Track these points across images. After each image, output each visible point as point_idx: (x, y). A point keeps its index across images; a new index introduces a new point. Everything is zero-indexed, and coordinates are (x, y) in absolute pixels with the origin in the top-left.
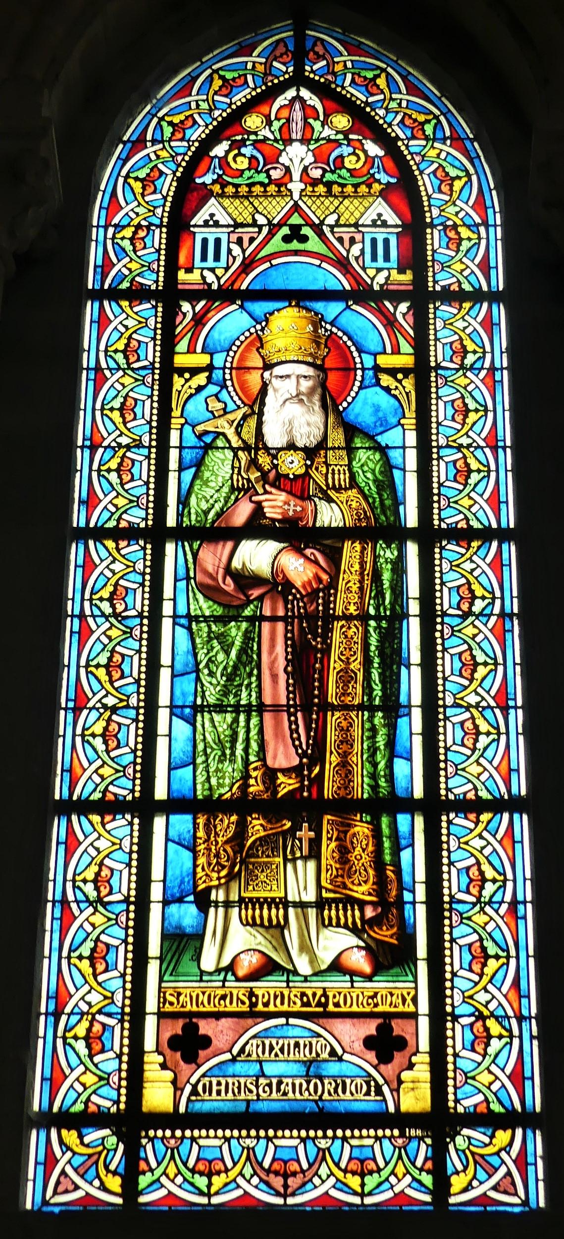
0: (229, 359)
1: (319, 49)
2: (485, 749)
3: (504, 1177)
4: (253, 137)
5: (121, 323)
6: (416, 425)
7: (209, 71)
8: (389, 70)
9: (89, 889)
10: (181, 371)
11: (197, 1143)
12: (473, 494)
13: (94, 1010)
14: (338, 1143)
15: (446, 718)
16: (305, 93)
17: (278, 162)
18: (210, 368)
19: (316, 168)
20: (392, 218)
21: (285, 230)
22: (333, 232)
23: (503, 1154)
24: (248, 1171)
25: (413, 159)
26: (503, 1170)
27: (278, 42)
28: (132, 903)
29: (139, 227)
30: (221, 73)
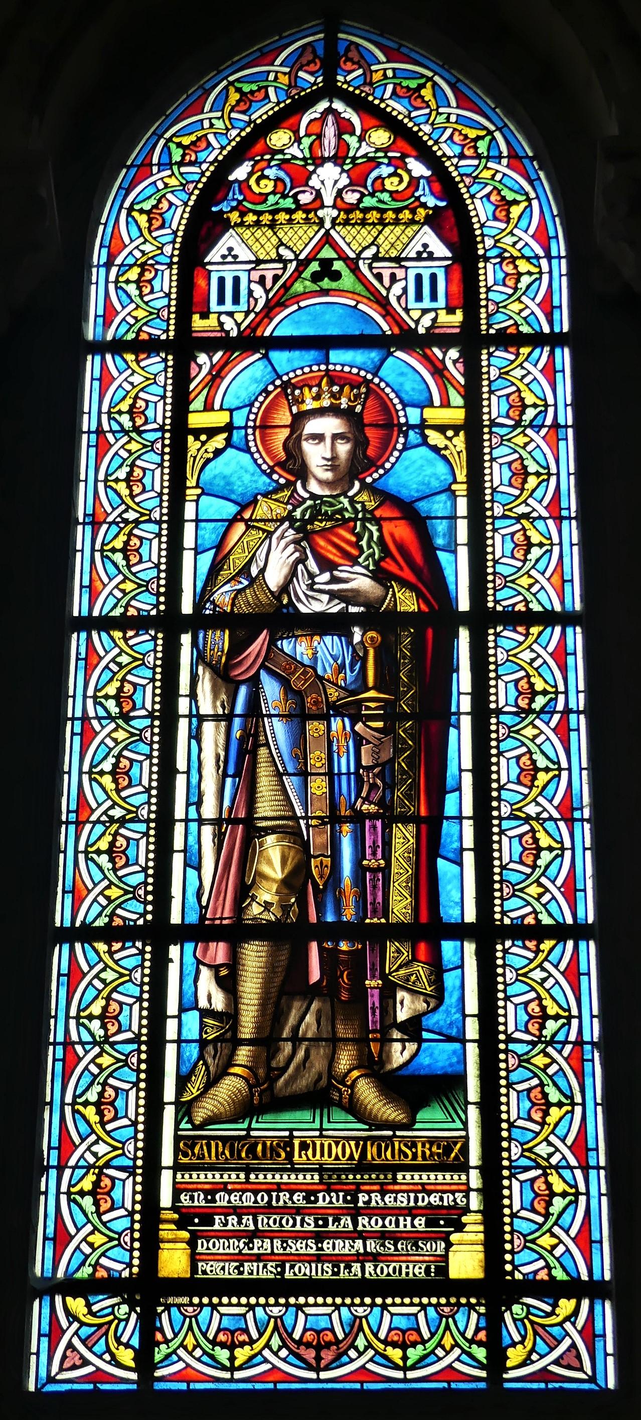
0: (252, 417)
1: (353, 54)
2: (547, 866)
3: (568, 1350)
4: (280, 156)
5: (126, 380)
6: (468, 490)
7: (225, 83)
8: (437, 79)
9: (125, 420)
10: (197, 433)
11: (218, 1312)
12: (543, 880)
13: (101, 1163)
14: (377, 1310)
15: (502, 832)
16: (338, 105)
17: (307, 185)
18: (229, 428)
19: (353, 191)
20: (440, 249)
21: (315, 266)
22: (371, 268)
23: (568, 1326)
24: (276, 1342)
25: (462, 181)
26: (567, 1342)
27: (304, 47)
28: (168, 431)
29: (143, 266)
30: (238, 85)
